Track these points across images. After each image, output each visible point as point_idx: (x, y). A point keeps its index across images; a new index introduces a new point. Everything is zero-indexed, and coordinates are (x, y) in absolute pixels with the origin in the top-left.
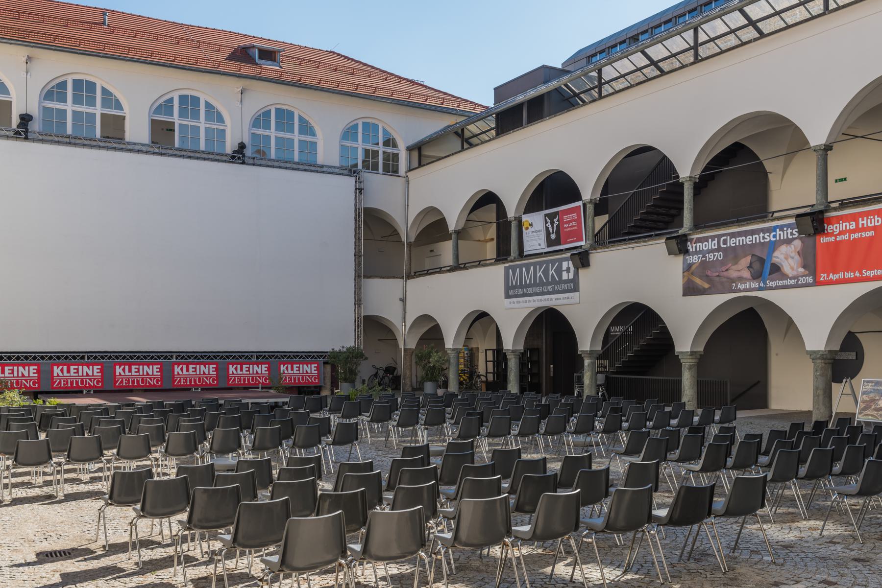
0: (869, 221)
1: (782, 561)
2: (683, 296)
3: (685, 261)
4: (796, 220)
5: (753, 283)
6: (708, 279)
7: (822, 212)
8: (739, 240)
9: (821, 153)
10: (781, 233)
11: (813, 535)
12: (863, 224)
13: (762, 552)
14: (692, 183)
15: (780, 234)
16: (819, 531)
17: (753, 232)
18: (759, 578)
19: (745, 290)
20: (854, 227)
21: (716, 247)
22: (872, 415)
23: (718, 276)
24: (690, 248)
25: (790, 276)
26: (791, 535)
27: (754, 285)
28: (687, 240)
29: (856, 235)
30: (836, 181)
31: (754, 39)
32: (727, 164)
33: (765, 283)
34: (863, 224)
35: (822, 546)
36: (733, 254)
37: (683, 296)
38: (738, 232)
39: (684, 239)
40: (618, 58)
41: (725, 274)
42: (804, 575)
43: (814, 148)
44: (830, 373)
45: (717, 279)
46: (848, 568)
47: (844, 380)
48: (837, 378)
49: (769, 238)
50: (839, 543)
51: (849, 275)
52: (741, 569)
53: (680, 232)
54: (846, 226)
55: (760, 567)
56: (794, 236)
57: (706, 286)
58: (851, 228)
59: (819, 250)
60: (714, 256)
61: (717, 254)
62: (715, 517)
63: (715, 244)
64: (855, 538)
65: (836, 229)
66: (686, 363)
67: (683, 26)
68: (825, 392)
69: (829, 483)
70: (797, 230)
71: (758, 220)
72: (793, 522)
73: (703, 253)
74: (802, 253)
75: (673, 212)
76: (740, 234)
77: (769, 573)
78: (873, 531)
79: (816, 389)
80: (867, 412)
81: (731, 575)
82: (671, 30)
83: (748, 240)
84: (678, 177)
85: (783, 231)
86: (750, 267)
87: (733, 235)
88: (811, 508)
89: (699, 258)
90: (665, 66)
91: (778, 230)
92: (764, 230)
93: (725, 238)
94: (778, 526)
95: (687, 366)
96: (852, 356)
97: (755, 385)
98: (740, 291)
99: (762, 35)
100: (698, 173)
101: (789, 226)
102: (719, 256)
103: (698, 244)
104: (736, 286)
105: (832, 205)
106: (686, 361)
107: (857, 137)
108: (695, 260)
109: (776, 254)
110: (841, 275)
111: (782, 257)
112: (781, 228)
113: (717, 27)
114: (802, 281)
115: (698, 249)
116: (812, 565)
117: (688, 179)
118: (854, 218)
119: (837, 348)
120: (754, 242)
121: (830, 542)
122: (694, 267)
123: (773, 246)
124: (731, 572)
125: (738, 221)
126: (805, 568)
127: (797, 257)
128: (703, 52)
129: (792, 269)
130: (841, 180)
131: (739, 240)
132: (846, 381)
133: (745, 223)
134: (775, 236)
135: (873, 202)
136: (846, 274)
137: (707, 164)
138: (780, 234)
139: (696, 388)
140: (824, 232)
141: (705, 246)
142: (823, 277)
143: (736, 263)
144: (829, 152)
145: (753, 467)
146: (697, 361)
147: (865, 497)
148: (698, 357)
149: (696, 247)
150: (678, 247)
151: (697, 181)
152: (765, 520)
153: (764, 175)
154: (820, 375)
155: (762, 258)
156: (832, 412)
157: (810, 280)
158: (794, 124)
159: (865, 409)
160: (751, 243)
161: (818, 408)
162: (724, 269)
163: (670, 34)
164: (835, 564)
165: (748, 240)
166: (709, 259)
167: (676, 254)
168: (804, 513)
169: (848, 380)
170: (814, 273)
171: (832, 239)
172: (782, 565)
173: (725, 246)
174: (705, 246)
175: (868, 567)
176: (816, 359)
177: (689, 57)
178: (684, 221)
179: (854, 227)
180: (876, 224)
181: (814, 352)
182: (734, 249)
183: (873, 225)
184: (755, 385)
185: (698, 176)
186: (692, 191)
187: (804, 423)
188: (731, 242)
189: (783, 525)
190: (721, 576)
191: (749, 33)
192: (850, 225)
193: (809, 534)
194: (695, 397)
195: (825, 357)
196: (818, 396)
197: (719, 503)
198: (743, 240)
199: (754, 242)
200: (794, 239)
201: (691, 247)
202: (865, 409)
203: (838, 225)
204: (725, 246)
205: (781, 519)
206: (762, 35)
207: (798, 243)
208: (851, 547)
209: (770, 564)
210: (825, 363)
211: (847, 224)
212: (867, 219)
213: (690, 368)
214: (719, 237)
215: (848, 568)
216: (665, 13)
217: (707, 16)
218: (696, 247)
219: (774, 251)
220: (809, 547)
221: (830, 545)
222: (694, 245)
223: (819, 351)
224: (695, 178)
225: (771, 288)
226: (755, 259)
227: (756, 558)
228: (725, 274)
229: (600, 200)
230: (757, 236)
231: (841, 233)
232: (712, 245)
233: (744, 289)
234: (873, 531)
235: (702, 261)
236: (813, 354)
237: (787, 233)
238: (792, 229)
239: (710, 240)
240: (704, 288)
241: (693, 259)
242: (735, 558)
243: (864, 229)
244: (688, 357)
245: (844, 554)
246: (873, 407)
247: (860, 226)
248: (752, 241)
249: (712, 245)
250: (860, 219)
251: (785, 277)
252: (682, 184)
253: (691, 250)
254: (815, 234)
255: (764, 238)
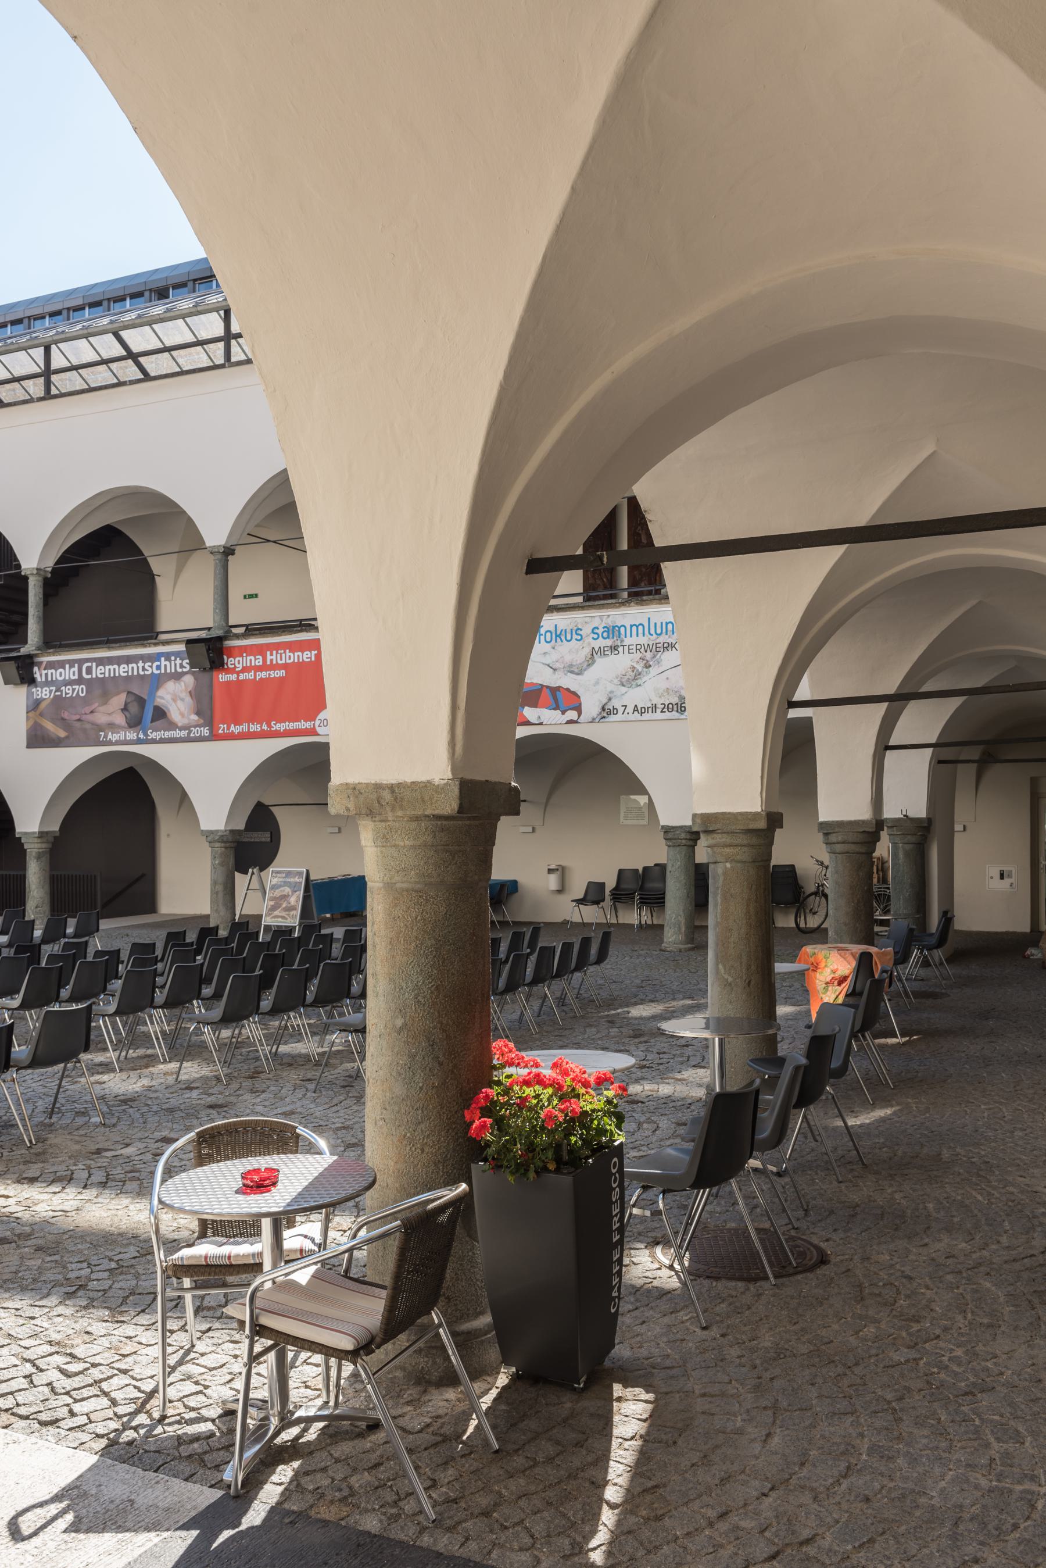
0: (279, 655)
1: (114, 1120)
2: (28, 747)
3: (29, 695)
4: (186, 647)
5: (130, 732)
6: (63, 723)
7: (220, 639)
8: (110, 670)
9: (219, 556)
10: (167, 663)
11: (168, 1082)
12: (271, 660)
13: (91, 1113)
14: (40, 579)
15: (165, 666)
16: (175, 1076)
17: (128, 660)
18: (77, 1147)
19: (118, 743)
20: (261, 663)
21: (76, 677)
22: (283, 917)
23: (79, 720)
24: (37, 676)
25: (180, 725)
26: (139, 1084)
27: (131, 735)
28: (32, 664)
29: (263, 675)
30: (245, 597)
31: (130, 381)
32: (96, 555)
33: (146, 734)
34: (271, 660)
35: (175, 1095)
36: (102, 688)
37: (28, 747)
38: (108, 658)
39: (28, 661)
40: (16, 346)
41: (90, 717)
42: (139, 1135)
43: (210, 549)
44: (232, 861)
45: (78, 725)
46: (198, 1118)
47: (250, 871)
48: (242, 867)
49: (151, 669)
50: (197, 1088)
51: (255, 728)
52: (53, 1139)
53: (22, 650)
54: (251, 660)
55: (82, 1132)
56: (184, 670)
57: (62, 734)
58: (257, 664)
59: (217, 692)
60: (74, 690)
61: (77, 687)
62: (17, 1070)
63: (74, 672)
64: (218, 1079)
65: (290, 657)
66: (32, 848)
67: (28, 340)
68: (225, 888)
69: (296, 1020)
70: (188, 661)
71: (136, 643)
72: (146, 1067)
73: (58, 685)
74: (195, 694)
75: (16, 618)
76: (110, 661)
77: (93, 1139)
78: (246, 1067)
79: (214, 883)
80: (276, 913)
81: (38, 1148)
82: (9, 341)
83: (122, 670)
84: (19, 566)
85: (170, 661)
86: (125, 709)
87: (101, 662)
88: (178, 1046)
89: (51, 692)
90: (154, 365)
91: (163, 659)
92: (145, 658)
93: (89, 664)
94: (124, 1075)
95: (34, 854)
96: (265, 837)
97: (138, 880)
98: (110, 743)
99: (147, 377)
100: (50, 563)
101: (177, 654)
102: (81, 690)
103: (50, 671)
104: (106, 736)
105: (235, 631)
106: (32, 846)
107: (268, 541)
108: (46, 695)
109: (161, 693)
110: (244, 728)
111: (168, 697)
112: (168, 656)
113: (81, 351)
114: (195, 732)
115: (50, 679)
116: (152, 1120)
117: (222, 550)
118: (261, 650)
119: (241, 826)
120: (130, 674)
121: (186, 1088)
122: (43, 705)
123: (157, 681)
124: (40, 1145)
125: (108, 642)
126: (142, 1125)
127: (188, 699)
128: (61, 382)
129: (182, 715)
130: (251, 596)
131: (110, 670)
132: (253, 873)
133: (118, 645)
134: (158, 668)
135: (284, 632)
136: (251, 726)
137: (64, 553)
138: (165, 666)
139: (47, 887)
140: (223, 666)
141: (61, 675)
142: (222, 729)
143: (105, 703)
144: (230, 557)
145: (102, 996)
146: (50, 846)
147: (234, 1024)
148: (52, 839)
149: (46, 675)
150: (20, 675)
151: (49, 575)
152: (106, 1067)
153: (148, 579)
154: (219, 864)
155: (142, 698)
156: (235, 915)
157: (206, 732)
158: (184, 512)
159: (273, 908)
160: (126, 674)
161: (217, 910)
162: (88, 710)
163: (8, 348)
164: (184, 1115)
165: (121, 670)
166: (66, 694)
167: (15, 684)
168: (163, 1055)
169: (255, 870)
170: (210, 723)
171: (234, 677)
172: (114, 1125)
173: (90, 676)
174: (61, 675)
175: (224, 1114)
176: (214, 842)
177: (36, 388)
178: (29, 634)
179: (261, 663)
180: (288, 661)
181: (212, 832)
182: (102, 681)
183: (283, 662)
184: (138, 880)
185: (50, 569)
186: (41, 590)
187: (185, 931)
188: (98, 672)
189: (132, 1073)
190: (23, 1151)
191: (128, 370)
192: (256, 659)
193: (163, 1081)
194: (47, 900)
195: (225, 839)
196: (217, 893)
197: (20, 1050)
198: (114, 669)
199: (130, 674)
200: (184, 674)
201: (39, 674)
202: (273, 908)
203: (241, 659)
204: (90, 676)
205: (132, 1065)
206: (147, 377)
207: (189, 680)
208: (211, 1091)
209: (97, 1127)
210: (226, 848)
211: (252, 658)
212: (277, 653)
213: (39, 857)
214: (81, 662)
215: (198, 1118)
216: (11, 308)
217: (63, 332)
218: (46, 675)
219: (157, 688)
220: (156, 1098)
221: (185, 1091)
222: (44, 672)
223: (217, 831)
224: (45, 571)
225: (154, 741)
226: (131, 698)
227: (80, 1121)
228: (90, 717)
229: (52, 572)
230: (134, 665)
231: (245, 669)
232: (70, 673)
233: (116, 741)
234: (246, 1067)
235: (55, 696)
236: (208, 834)
237: (175, 665)
238: (182, 659)
239: (67, 666)
240: (59, 738)
241: (42, 692)
242: (52, 1125)
243: (274, 667)
244: (36, 840)
245: (199, 1102)
246: (284, 905)
247: (268, 663)
248: (128, 672)
249: (70, 673)
250: (268, 653)
251: (172, 726)
252: (26, 578)
253: (39, 679)
254: (211, 668)
255: (144, 669)
